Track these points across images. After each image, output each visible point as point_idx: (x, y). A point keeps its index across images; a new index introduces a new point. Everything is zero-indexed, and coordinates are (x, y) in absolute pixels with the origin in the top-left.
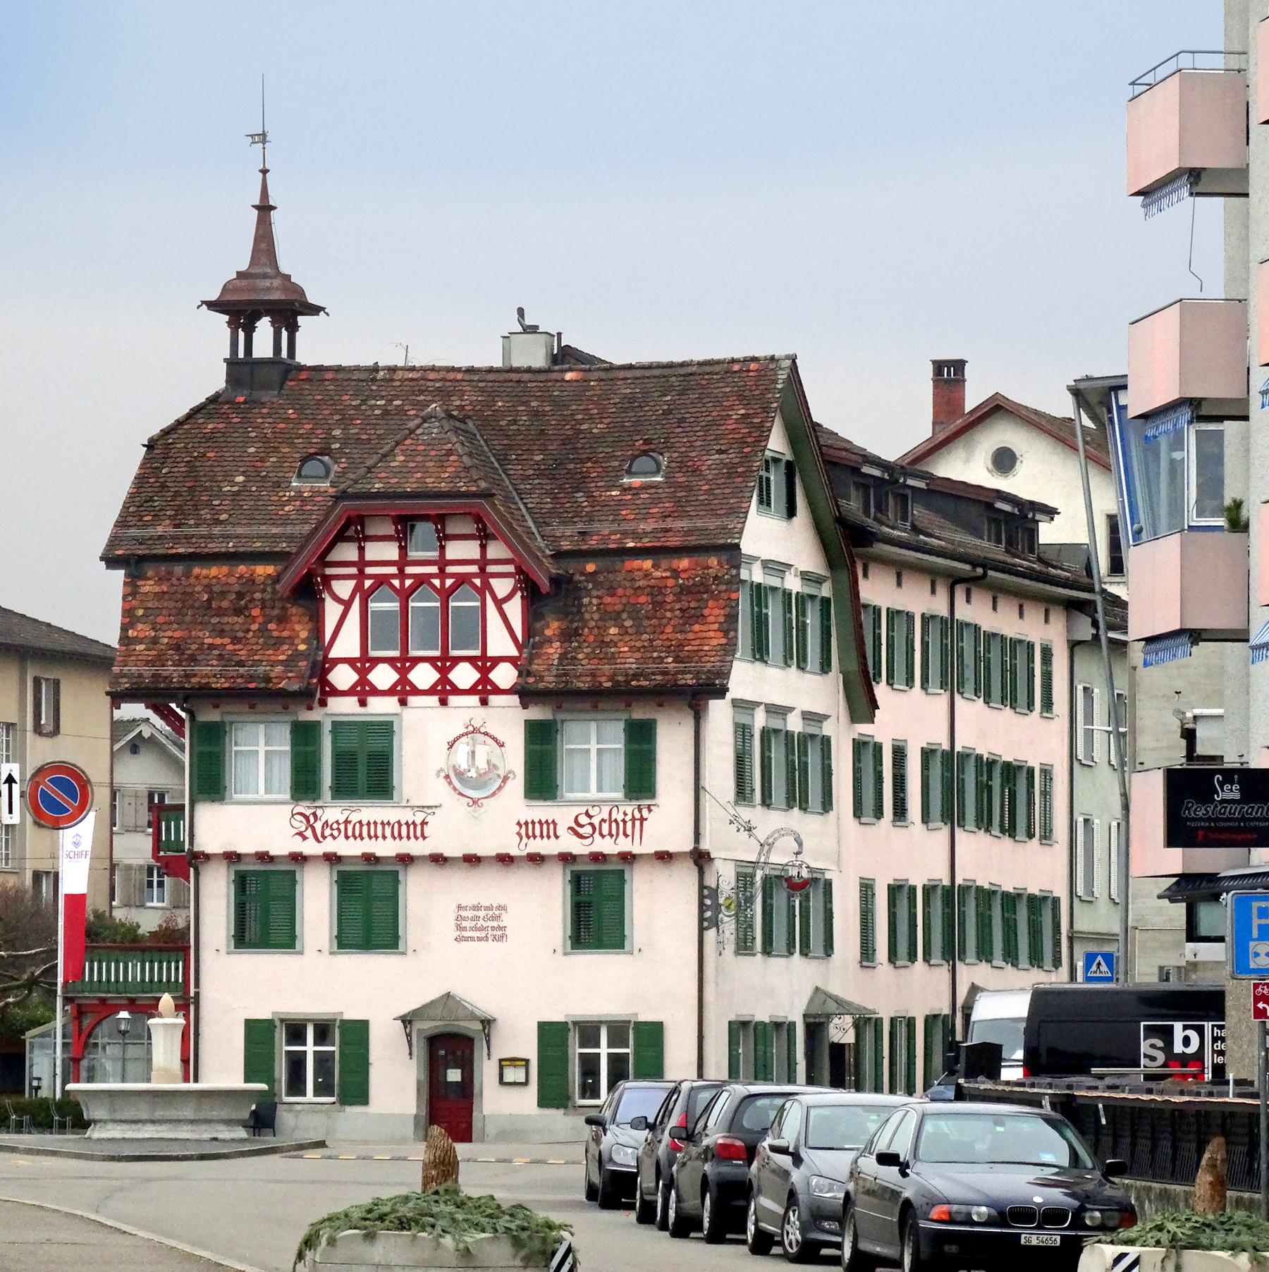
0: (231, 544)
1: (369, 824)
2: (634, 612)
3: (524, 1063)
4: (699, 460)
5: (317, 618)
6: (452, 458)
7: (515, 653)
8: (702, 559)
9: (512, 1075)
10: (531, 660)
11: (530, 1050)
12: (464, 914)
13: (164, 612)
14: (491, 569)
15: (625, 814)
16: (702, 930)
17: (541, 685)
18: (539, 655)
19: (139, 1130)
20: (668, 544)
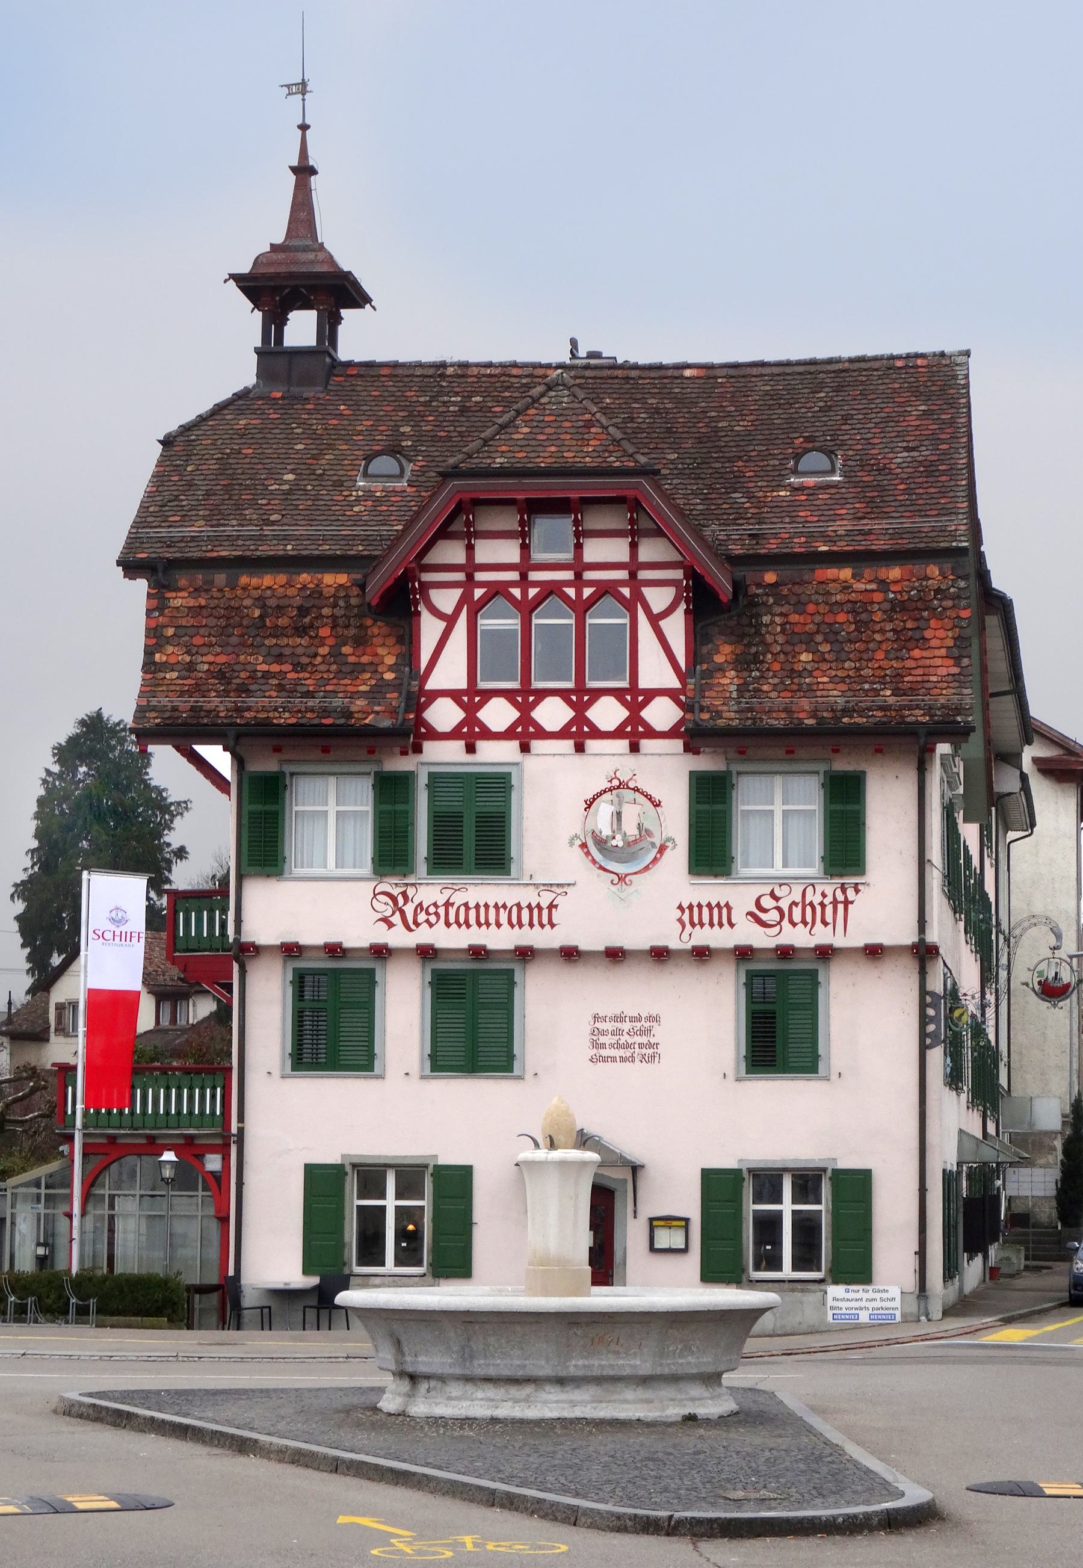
0: (289, 547)
1: (477, 907)
2: (832, 635)
3: (683, 1223)
4: (884, 458)
5: (410, 640)
6: (593, 430)
7: (674, 683)
8: (917, 568)
9: (666, 1238)
10: (701, 690)
11: (690, 1205)
12: (601, 1026)
13: (202, 631)
14: (644, 575)
15: (824, 895)
16: (923, 1049)
17: (721, 722)
18: (710, 687)
19: (527, 1400)
20: (874, 547)
